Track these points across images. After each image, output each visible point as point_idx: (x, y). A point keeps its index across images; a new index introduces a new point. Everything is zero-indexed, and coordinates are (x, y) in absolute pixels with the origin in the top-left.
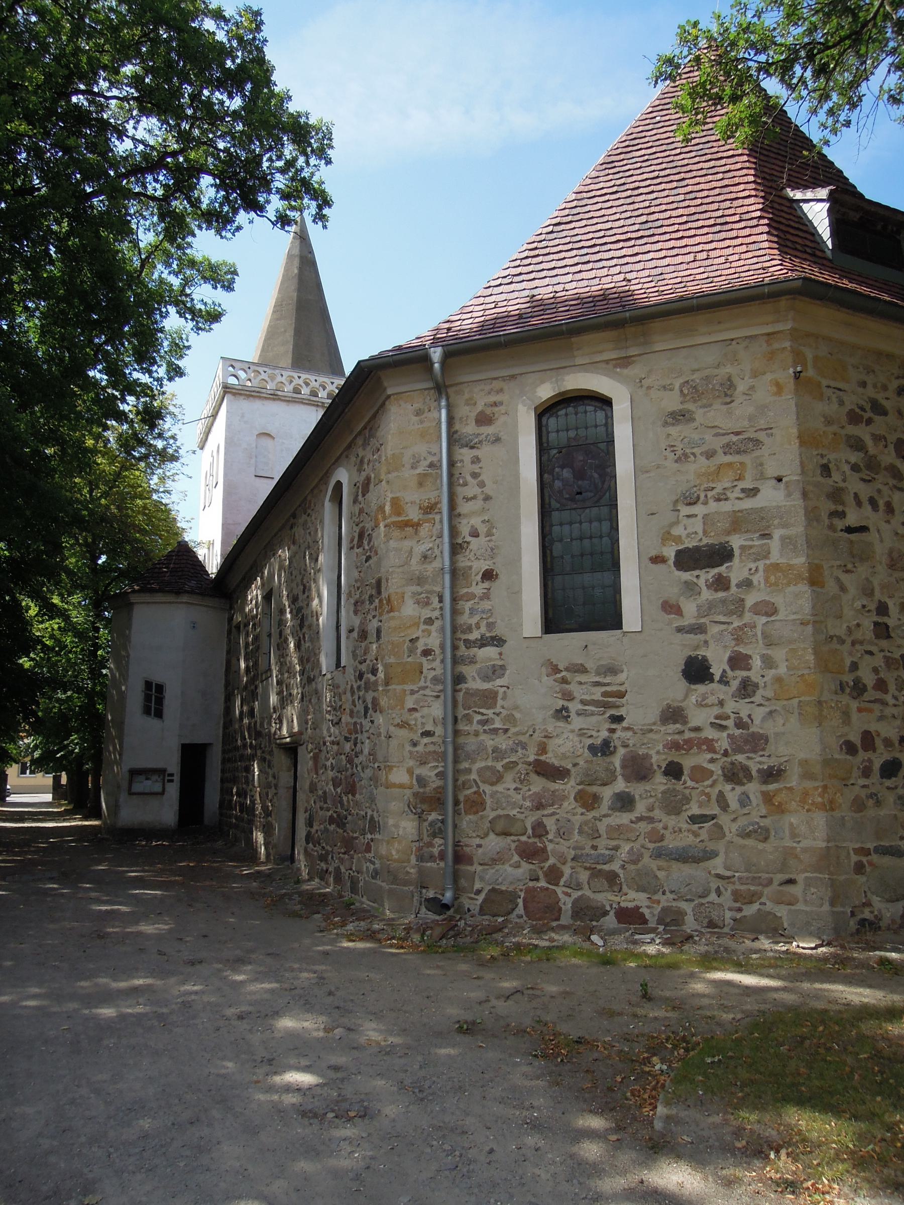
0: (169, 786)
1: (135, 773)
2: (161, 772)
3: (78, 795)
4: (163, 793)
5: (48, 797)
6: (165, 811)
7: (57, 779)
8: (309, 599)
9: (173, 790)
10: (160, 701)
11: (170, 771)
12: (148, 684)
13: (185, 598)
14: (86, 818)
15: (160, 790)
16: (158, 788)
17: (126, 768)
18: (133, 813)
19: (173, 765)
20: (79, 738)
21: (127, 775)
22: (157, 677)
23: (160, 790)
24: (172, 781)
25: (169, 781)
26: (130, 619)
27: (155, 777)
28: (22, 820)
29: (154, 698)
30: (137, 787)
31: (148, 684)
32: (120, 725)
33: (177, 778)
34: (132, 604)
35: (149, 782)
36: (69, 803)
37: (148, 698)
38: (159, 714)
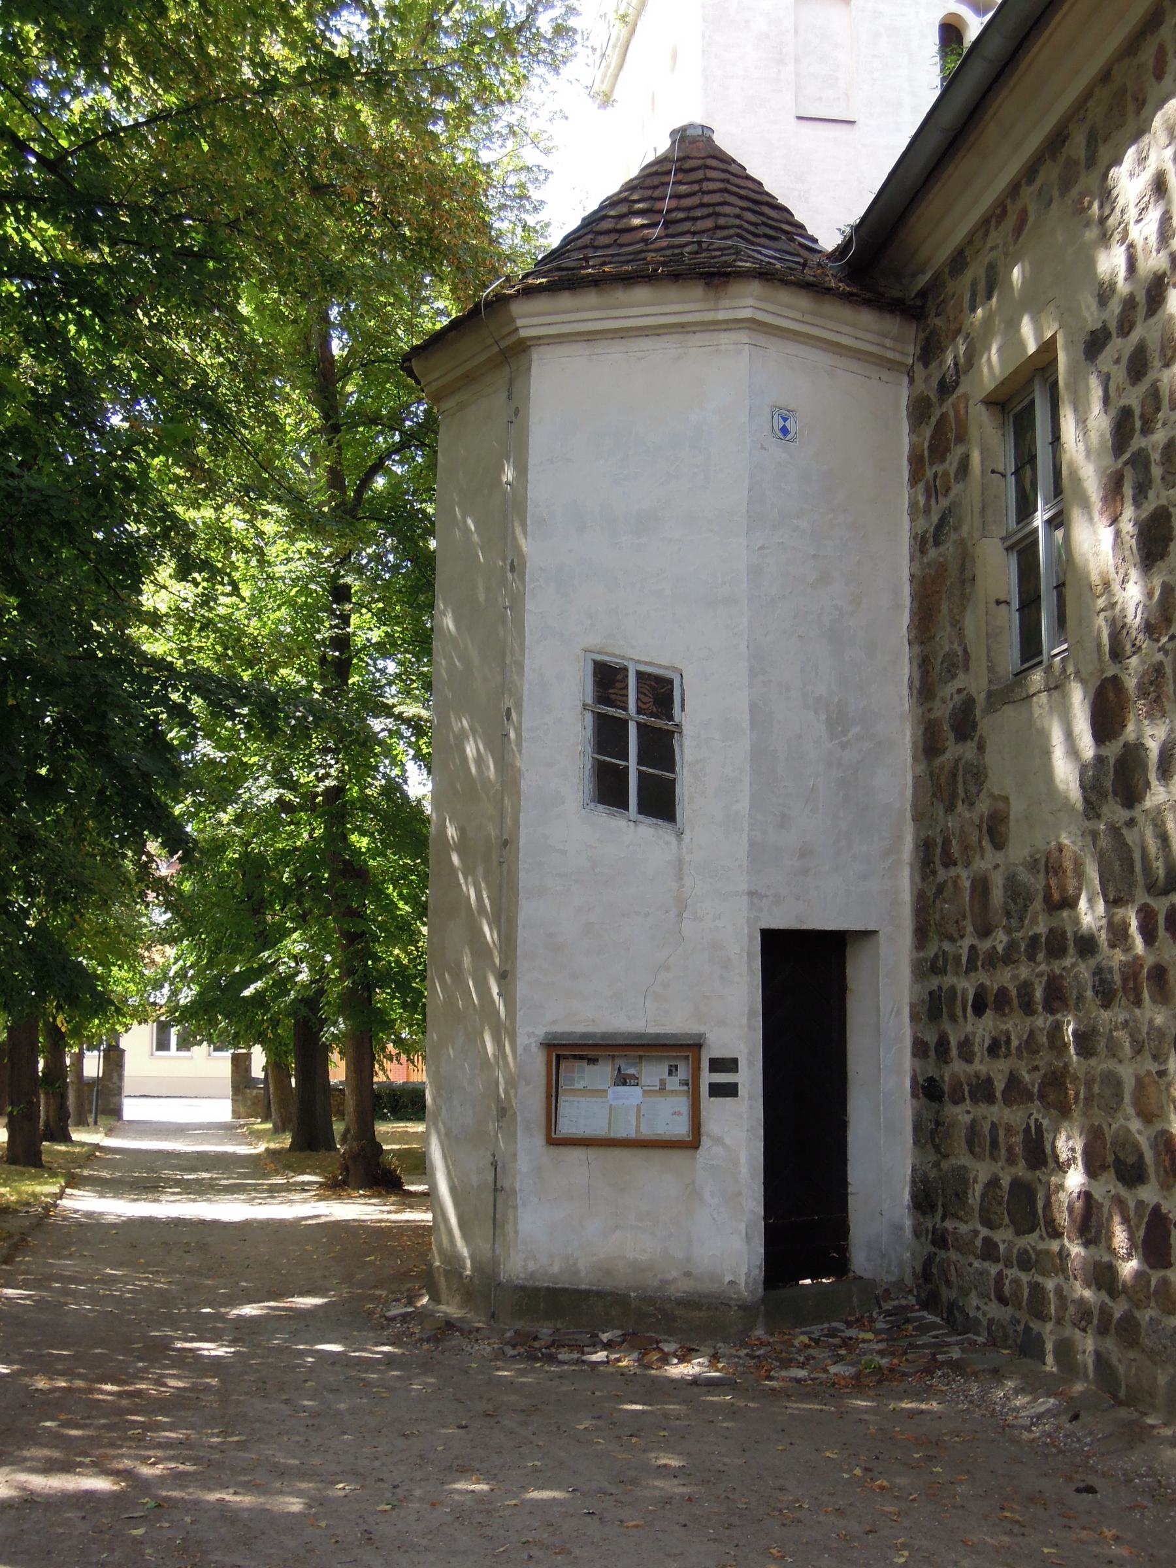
0: (715, 1111)
1: (567, 1052)
2: (681, 1050)
3: (321, 1119)
4: (693, 1143)
5: (222, 1110)
6: (707, 1221)
7: (241, 1065)
8: (28, 1179)
9: (738, 1130)
10: (660, 747)
11: (716, 1047)
12: (607, 678)
13: (747, 302)
14: (335, 1188)
15: (680, 1128)
16: (669, 1118)
17: (530, 1033)
18: (567, 1227)
19: (733, 1020)
20: (310, 940)
21: (538, 1062)
22: (643, 649)
23: (680, 1128)
24: (730, 1090)
25: (718, 1090)
26: (517, 414)
27: (653, 1073)
28: (149, 1187)
29: (636, 746)
30: (579, 1116)
31: (607, 678)
32: (498, 856)
33: (750, 1078)
34: (522, 348)
35: (632, 1095)
36: (277, 1130)
37: (609, 735)
38: (660, 803)
